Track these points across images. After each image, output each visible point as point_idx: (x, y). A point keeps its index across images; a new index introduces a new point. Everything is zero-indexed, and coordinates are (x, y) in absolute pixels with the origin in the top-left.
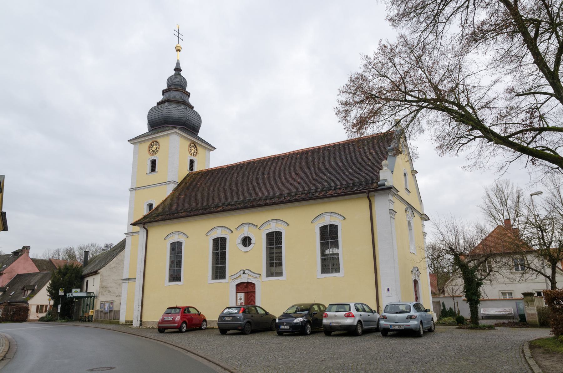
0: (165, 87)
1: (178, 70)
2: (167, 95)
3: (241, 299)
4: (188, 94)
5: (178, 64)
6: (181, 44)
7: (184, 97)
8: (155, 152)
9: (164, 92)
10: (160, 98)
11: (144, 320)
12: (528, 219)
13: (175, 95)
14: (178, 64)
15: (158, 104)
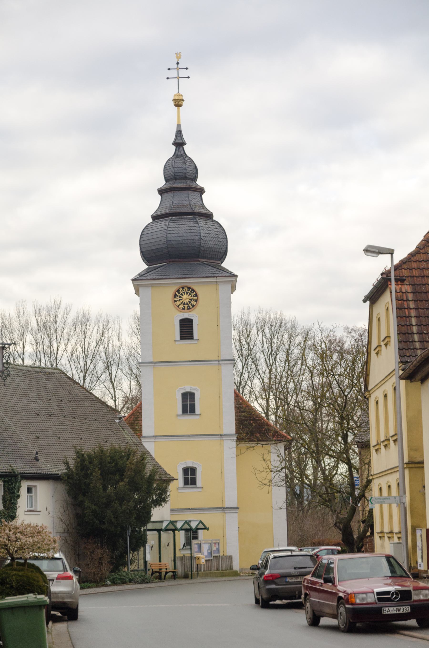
1: (179, 144)
8: (190, 306)
10: (154, 203)
11: (224, 441)
13: (180, 200)
15: (155, 218)
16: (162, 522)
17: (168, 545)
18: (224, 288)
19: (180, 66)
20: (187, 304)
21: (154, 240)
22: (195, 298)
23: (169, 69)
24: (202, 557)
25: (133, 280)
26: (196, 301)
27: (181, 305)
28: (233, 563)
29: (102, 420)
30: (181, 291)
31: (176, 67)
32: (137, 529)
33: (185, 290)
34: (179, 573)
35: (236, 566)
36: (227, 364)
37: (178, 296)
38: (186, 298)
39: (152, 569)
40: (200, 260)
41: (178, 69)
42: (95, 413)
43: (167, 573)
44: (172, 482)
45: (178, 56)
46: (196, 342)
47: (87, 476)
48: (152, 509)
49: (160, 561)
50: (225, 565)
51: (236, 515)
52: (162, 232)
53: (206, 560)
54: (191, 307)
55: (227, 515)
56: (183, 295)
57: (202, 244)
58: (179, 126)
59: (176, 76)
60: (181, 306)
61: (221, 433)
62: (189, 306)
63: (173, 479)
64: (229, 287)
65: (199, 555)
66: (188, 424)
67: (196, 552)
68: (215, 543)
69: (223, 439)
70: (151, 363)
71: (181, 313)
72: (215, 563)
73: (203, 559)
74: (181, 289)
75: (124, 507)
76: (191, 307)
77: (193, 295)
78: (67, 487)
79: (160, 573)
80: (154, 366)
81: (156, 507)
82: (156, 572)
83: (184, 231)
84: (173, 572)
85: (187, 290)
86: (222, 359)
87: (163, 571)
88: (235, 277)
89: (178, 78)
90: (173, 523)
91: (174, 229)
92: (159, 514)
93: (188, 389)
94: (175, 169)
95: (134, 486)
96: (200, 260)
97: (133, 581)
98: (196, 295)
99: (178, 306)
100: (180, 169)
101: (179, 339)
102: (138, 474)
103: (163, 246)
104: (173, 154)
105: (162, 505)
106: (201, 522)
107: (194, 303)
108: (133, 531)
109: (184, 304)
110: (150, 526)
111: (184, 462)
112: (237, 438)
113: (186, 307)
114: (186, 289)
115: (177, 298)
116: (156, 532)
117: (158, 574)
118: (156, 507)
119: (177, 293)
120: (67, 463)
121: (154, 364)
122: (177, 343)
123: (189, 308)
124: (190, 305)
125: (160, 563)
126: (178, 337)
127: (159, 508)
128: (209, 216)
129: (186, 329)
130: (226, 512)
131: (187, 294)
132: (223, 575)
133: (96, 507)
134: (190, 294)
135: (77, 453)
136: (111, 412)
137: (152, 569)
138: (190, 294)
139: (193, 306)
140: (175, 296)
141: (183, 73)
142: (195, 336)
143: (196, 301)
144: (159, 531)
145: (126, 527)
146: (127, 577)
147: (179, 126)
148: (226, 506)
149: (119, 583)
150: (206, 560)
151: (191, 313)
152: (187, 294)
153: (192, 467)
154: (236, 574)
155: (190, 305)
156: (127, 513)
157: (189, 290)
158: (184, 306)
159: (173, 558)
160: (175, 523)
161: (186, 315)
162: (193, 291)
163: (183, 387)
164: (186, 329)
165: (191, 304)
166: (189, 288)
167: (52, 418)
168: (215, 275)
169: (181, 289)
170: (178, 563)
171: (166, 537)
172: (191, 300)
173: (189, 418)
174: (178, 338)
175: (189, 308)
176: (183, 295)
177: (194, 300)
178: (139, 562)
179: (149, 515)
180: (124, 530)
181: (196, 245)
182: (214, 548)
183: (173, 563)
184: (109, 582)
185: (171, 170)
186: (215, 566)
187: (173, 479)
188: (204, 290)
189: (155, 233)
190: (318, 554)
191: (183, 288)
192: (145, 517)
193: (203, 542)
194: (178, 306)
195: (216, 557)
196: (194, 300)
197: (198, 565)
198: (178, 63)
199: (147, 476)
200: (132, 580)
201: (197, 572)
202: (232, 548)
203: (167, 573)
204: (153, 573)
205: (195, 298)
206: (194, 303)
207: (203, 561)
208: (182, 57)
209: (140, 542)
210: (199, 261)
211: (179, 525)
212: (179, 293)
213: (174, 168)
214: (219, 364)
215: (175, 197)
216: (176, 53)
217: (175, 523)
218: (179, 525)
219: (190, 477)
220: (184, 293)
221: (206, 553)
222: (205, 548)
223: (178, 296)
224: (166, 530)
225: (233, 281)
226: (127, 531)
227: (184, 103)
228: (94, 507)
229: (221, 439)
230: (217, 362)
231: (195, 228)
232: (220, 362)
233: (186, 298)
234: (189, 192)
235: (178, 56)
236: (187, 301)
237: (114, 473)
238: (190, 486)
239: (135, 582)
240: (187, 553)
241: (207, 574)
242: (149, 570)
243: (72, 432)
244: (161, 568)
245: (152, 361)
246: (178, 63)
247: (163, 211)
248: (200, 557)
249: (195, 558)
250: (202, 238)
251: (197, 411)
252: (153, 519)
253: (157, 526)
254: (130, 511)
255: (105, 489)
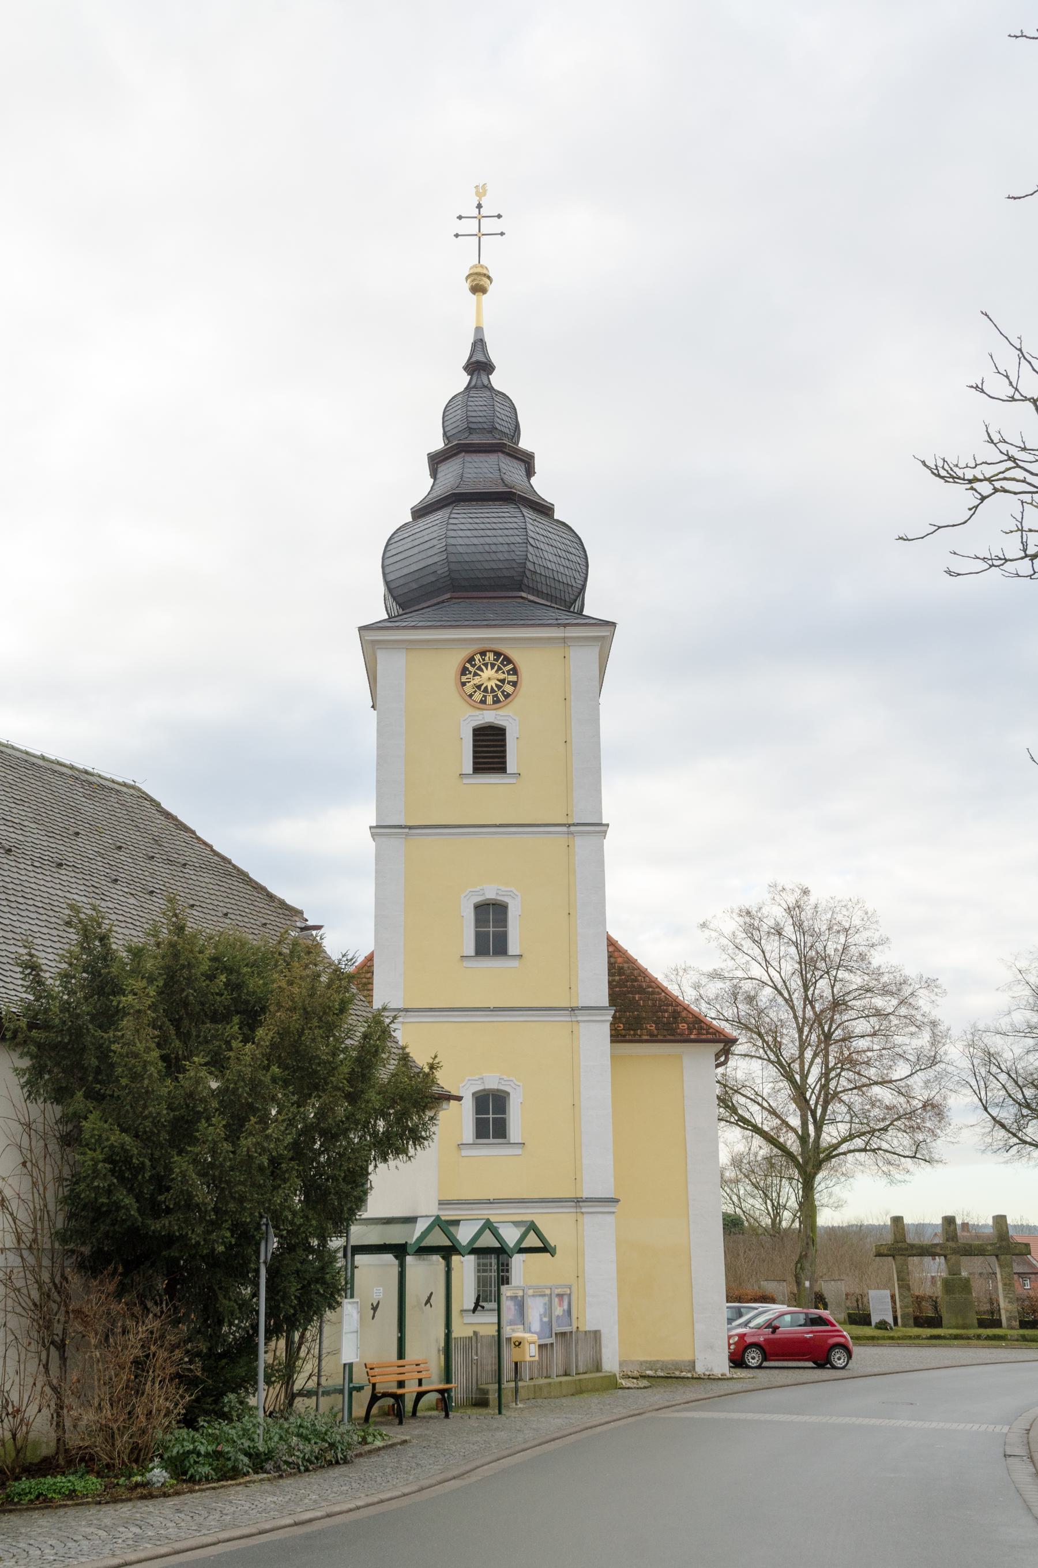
0: (438, 444)
1: (479, 366)
2: (450, 471)
3: (59, 1321)
4: (527, 461)
5: (479, 344)
6: (491, 264)
7: (514, 472)
8: (499, 697)
9: (436, 461)
10: (420, 486)
11: (581, 1024)
12: (725, 1086)
13: (482, 471)
14: (479, 344)
15: (420, 512)
16: (411, 1220)
17: (428, 1301)
18: (583, 657)
19: (483, 212)
20: (493, 691)
21: (416, 550)
22: (513, 678)
23: (460, 218)
24: (528, 1337)
25: (360, 629)
26: (514, 684)
27: (477, 693)
28: (604, 1350)
29: (246, 920)
30: (477, 662)
31: (475, 212)
32: (315, 1242)
33: (487, 658)
34: (459, 1386)
35: (611, 1363)
36: (588, 833)
37: (470, 673)
38: (489, 677)
39: (374, 1385)
40: (524, 595)
41: (479, 218)
42: (227, 900)
43: (420, 1395)
44: (445, 1105)
45: (481, 191)
46: (513, 781)
47: (108, 1019)
48: (371, 1168)
49: (401, 1355)
50: (583, 1358)
51: (610, 1219)
52: (436, 528)
53: (540, 1346)
54: (502, 698)
55: (587, 1219)
56: (482, 671)
57: (529, 556)
58: (479, 330)
59: (476, 231)
60: (478, 696)
61: (574, 1005)
62: (496, 696)
63: (449, 1097)
64: (592, 654)
65: (519, 1334)
66: (490, 981)
67: (511, 1323)
68: (560, 1296)
69: (579, 1018)
70: (400, 827)
71: (478, 712)
72: (558, 1355)
73: (532, 1346)
74: (478, 657)
75: (247, 1142)
76: (502, 698)
77: (508, 672)
78: (26, 1063)
79: (399, 1398)
80: (407, 835)
81: (385, 1160)
82: (385, 1395)
83: (489, 526)
84: (441, 1392)
85: (492, 658)
86: (576, 821)
87: (411, 1389)
88: (608, 628)
89: (479, 235)
90: (445, 1225)
91: (463, 521)
92: (399, 1189)
93: (490, 893)
94: (470, 408)
95: (303, 1071)
96: (524, 595)
97: (268, 1466)
98: (515, 671)
99: (471, 696)
100: (481, 408)
101: (471, 771)
102: (315, 1022)
103: (436, 559)
104: (465, 385)
105: (405, 1151)
106: (532, 1227)
107: (509, 688)
108: (288, 1248)
109: (486, 690)
110: (358, 1234)
111: (476, 1077)
112: (614, 1017)
113: (490, 699)
114: (490, 656)
115: (468, 676)
116: (389, 1258)
117: (391, 1401)
118: (385, 1160)
119: (468, 665)
120: (32, 968)
121: (407, 830)
122: (466, 781)
123: (497, 701)
124: (500, 694)
125: (401, 1362)
126: (468, 766)
127: (397, 1161)
128: (544, 510)
129: (490, 750)
130: (583, 1210)
131: (492, 668)
132: (579, 1390)
133: (127, 1139)
134: (499, 669)
135: (86, 934)
136: (280, 911)
137: (374, 1385)
138: (499, 669)
139: (507, 696)
140: (464, 671)
141: (488, 226)
142: (511, 765)
143: (514, 684)
144: (399, 1251)
145: (258, 1227)
146: (247, 1444)
147: (479, 330)
148: (585, 1195)
149: (208, 1480)
150: (540, 1346)
151: (500, 712)
152: (492, 668)
153: (498, 1090)
154: (611, 1384)
155: (500, 694)
156: (261, 1169)
157: (496, 660)
158: (485, 697)
159: (442, 1344)
160: (452, 1229)
161: (489, 717)
162: (508, 660)
163: (478, 888)
164: (490, 750)
165: (503, 692)
166: (498, 654)
167: (63, 872)
168: (559, 622)
169: (478, 657)
170: (457, 1358)
171: (424, 1273)
172: (503, 681)
173: (492, 964)
174: (468, 768)
175: (497, 701)
176: (482, 671)
177: (509, 683)
178: (323, 1363)
179: (354, 1187)
180: (247, 1237)
181: (515, 558)
182: (558, 1311)
183: (442, 1357)
184: (158, 1475)
185: (459, 412)
186: (560, 1361)
187: (449, 1097)
188: (537, 655)
189: (418, 535)
190: (776, 1323)
191: (483, 654)
192: (339, 1196)
193: (531, 1292)
194: (471, 696)
195: (563, 1334)
196: (509, 683)
197: (516, 1364)
198: (479, 206)
199: (352, 1042)
200: (269, 1456)
201: (513, 1384)
202: (599, 1312)
203: (420, 1395)
204: (374, 1398)
205: (513, 678)
206: (509, 688)
207: (531, 1353)
208: (488, 193)
209: (309, 1293)
210: (522, 598)
211: (464, 1235)
212: (473, 666)
213: (467, 406)
214: (568, 833)
215: (467, 465)
216: (477, 187)
217: (452, 1229)
218: (464, 1235)
219: (491, 1116)
220: (486, 665)
221: (536, 1326)
222: (535, 1311)
223: (470, 673)
224: (424, 1251)
225: (603, 637)
226: (258, 1244)
227: (492, 289)
228: (117, 1138)
229: (574, 1019)
230: (564, 829)
231: (515, 520)
232: (572, 829)
233: (489, 677)
234: (500, 454)
235: (481, 191)
236: (492, 684)
237: (220, 1017)
238: (491, 1140)
239: (278, 1468)
240: (485, 1324)
241: (540, 1387)
242: (359, 1389)
243: (130, 921)
244: (401, 1378)
245: (403, 823)
246: (479, 206)
247: (441, 491)
248: (523, 1338)
249: (509, 1339)
250: (531, 540)
251: (513, 948)
252: (376, 1206)
253: (395, 1235)
254: (272, 1161)
255: (173, 1065)
